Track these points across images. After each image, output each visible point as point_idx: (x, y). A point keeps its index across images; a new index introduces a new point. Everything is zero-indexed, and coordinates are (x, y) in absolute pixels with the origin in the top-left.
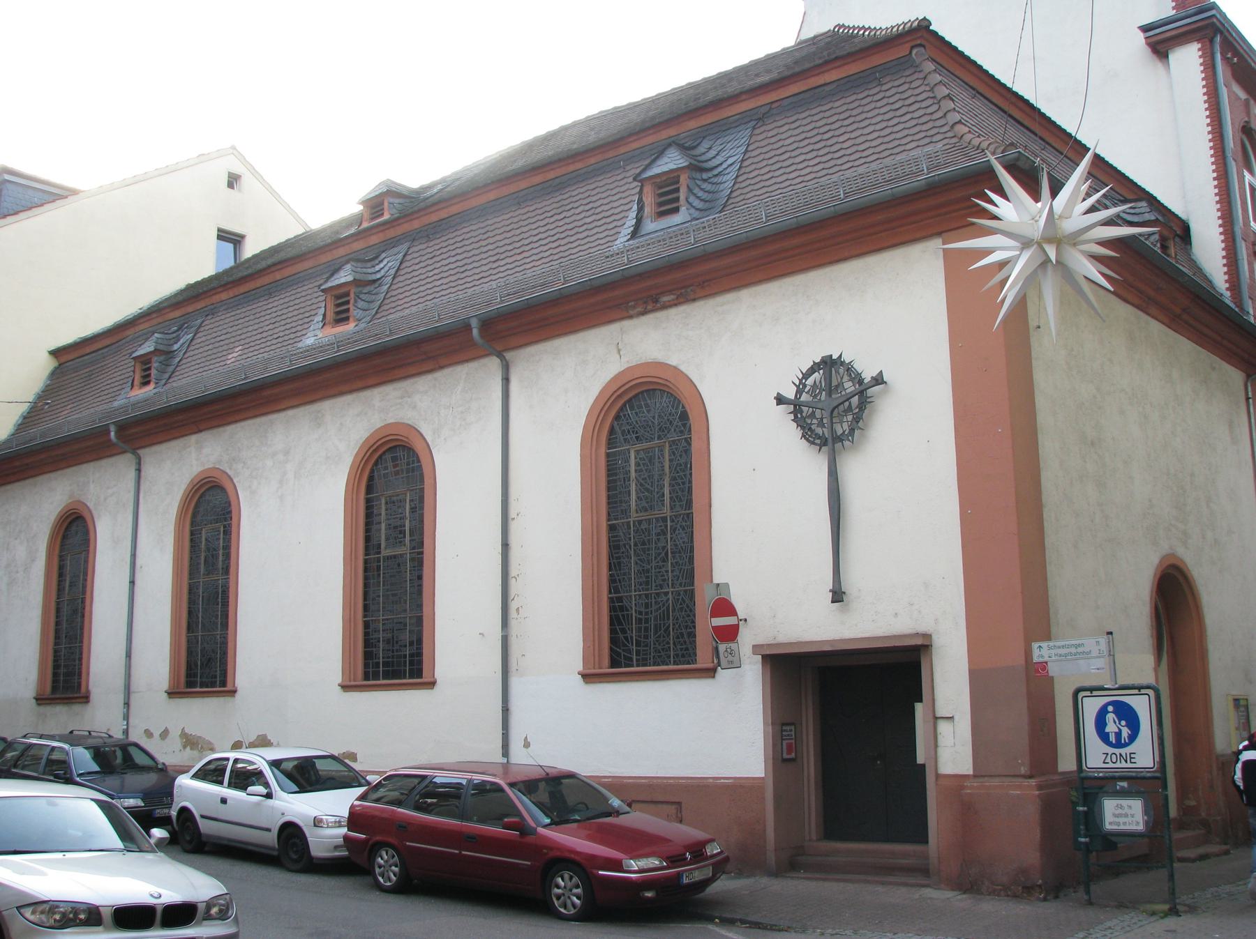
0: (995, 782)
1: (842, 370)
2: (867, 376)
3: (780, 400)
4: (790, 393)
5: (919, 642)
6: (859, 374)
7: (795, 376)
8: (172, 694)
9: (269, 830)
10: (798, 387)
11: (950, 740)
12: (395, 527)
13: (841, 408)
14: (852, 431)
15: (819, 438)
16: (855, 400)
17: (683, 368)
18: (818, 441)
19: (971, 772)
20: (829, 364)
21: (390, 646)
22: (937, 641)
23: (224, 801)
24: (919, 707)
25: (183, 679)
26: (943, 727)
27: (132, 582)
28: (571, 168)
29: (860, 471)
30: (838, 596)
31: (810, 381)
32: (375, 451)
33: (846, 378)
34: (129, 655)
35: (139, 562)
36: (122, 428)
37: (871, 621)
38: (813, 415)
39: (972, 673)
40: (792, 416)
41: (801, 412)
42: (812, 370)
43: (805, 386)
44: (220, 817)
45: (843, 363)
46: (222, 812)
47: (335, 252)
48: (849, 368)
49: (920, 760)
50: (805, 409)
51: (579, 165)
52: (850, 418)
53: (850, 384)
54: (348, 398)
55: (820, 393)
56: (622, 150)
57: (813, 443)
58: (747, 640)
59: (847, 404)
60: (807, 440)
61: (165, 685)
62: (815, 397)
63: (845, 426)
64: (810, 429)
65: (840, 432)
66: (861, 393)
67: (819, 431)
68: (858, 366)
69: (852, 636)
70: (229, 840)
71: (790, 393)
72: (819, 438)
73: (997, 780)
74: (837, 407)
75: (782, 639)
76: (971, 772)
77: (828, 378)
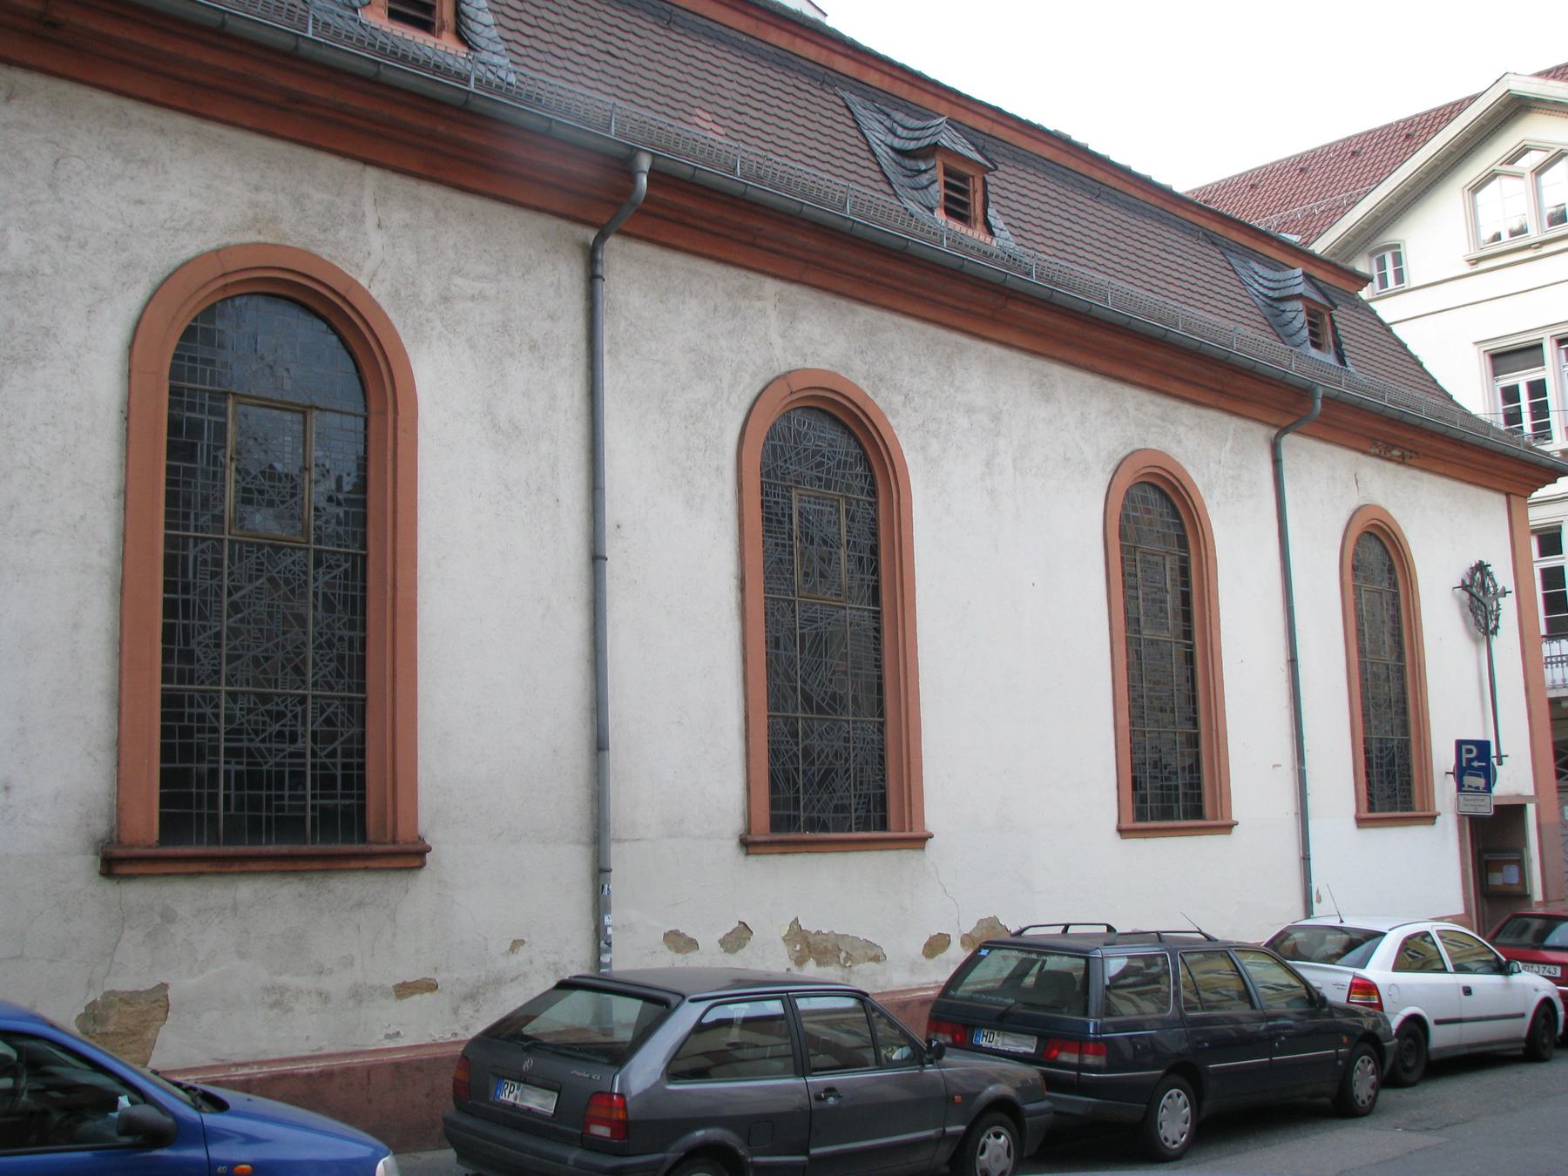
8: (749, 845)
9: (1522, 1015)
12: (1154, 601)
21: (1171, 781)
23: (1467, 991)
25: (1364, 804)
27: (596, 558)
28: (1132, 191)
32: (1175, 489)
34: (600, 745)
35: (613, 510)
36: (1330, 401)
44: (1465, 1015)
46: (1469, 1007)
47: (799, 42)
51: (1140, 195)
54: (1091, 380)
56: (1178, 212)
61: (735, 823)
70: (1469, 1046)
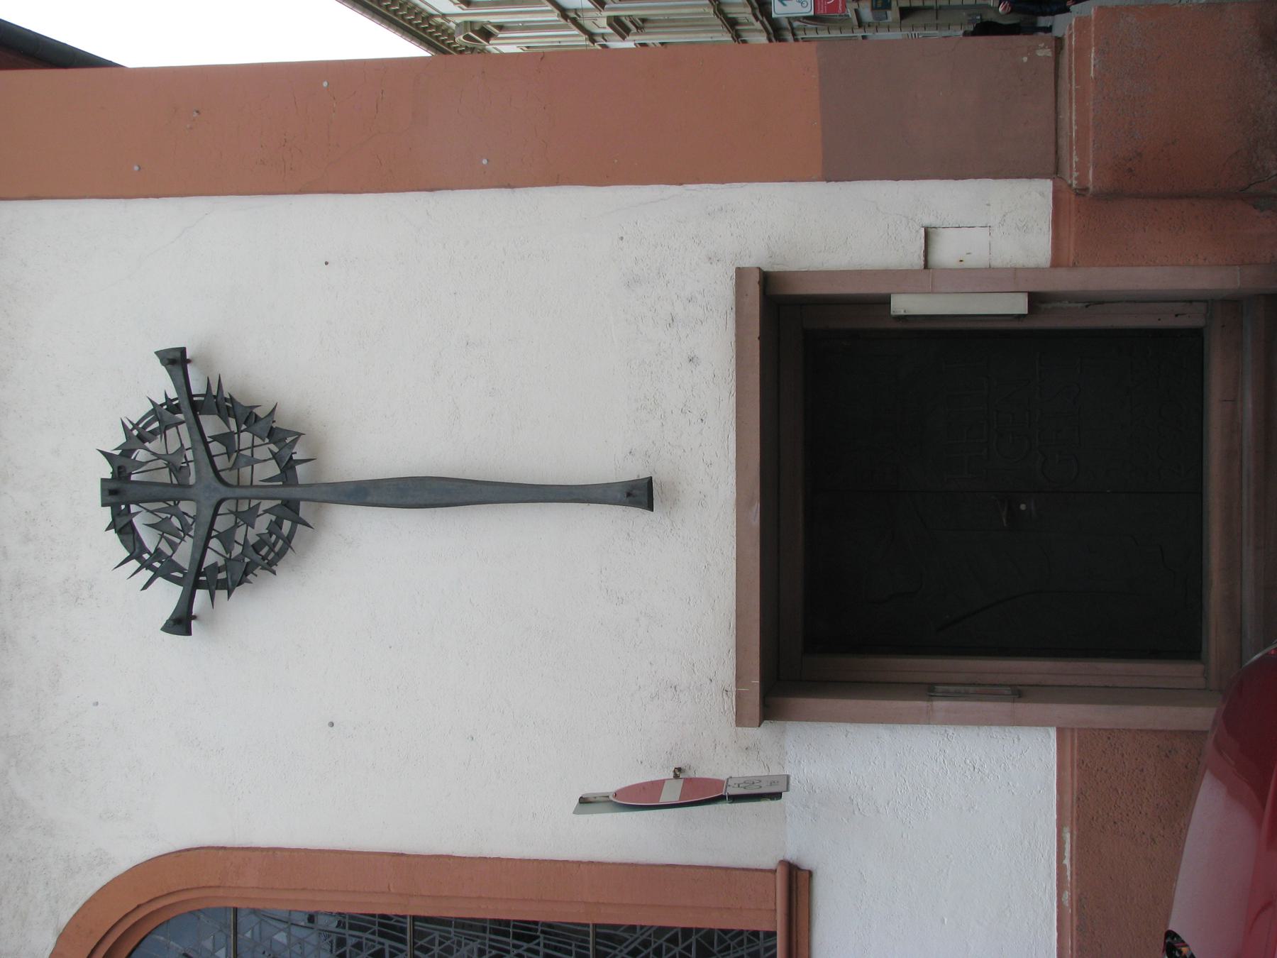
0: (1070, 116)
1: (141, 455)
2: (162, 386)
3: (181, 623)
4: (167, 596)
5: (754, 291)
6: (156, 411)
7: (131, 578)
10: (157, 573)
11: (969, 236)
13: (221, 462)
14: (274, 434)
15: (278, 523)
16: (212, 425)
17: (65, 918)
18: (287, 525)
19: (1046, 186)
20: (119, 491)
22: (758, 257)
24: (903, 304)
26: (948, 252)
29: (365, 442)
30: (640, 494)
31: (150, 539)
33: (156, 445)
37: (699, 422)
38: (227, 539)
39: (831, 175)
40: (221, 594)
41: (215, 568)
42: (124, 529)
43: (158, 554)
45: (126, 451)
48: (138, 435)
49: (1019, 305)
50: (210, 558)
52: (246, 438)
53: (171, 432)
55: (181, 516)
57: (288, 540)
58: (731, 753)
59: (216, 448)
60: (280, 555)
62: (185, 529)
63: (263, 452)
64: (256, 548)
65: (272, 469)
66: (197, 407)
67: (262, 524)
68: (138, 410)
69: (732, 480)
71: (167, 596)
72: (278, 523)
73: (1064, 116)
74: (216, 472)
75: (727, 674)
76: (1046, 186)
77: (149, 493)
